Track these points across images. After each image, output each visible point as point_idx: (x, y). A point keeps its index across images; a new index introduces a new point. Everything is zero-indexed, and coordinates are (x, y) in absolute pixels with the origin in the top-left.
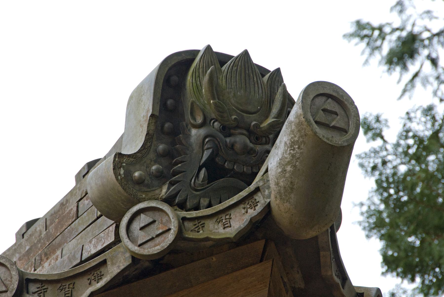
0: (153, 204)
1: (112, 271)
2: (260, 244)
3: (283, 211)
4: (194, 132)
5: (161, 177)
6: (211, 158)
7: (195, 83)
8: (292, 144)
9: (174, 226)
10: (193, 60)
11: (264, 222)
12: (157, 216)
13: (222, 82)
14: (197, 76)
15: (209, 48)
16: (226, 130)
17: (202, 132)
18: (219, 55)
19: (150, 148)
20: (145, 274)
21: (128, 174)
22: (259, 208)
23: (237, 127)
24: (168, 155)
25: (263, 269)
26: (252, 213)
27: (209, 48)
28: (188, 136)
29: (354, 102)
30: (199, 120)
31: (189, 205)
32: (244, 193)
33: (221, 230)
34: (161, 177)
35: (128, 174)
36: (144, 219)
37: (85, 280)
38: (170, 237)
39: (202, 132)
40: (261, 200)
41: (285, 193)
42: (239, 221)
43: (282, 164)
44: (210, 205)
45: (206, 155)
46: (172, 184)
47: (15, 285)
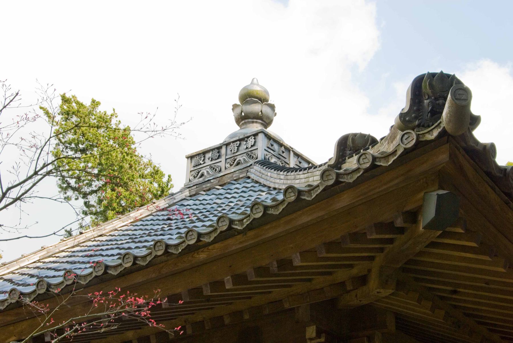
0: (408, 131)
1: (399, 153)
2: (446, 137)
3: (449, 129)
4: (425, 101)
5: (416, 118)
6: (432, 110)
7: (425, 85)
8: (449, 107)
9: (415, 137)
10: (424, 78)
11: (444, 133)
12: (410, 135)
13: (434, 83)
14: (425, 83)
15: (442, 72)
16: (436, 99)
17: (428, 101)
18: (431, 73)
19: (143, 218)
20: (407, 153)
21: (404, 119)
22: (441, 129)
23: (440, 97)
24: (418, 110)
25: (447, 146)
26: (439, 130)
27: (442, 72)
28: (424, 103)
29: (402, 116)
30: (427, 97)
31: (425, 125)
32: (436, 124)
33: (430, 137)
34: (416, 118)
35: (404, 119)
36: (406, 136)
37: (391, 157)
38: (414, 141)
39: (428, 101)
40: (442, 126)
41: (449, 121)
42: (435, 133)
43: (447, 114)
44: (433, 125)
45: (430, 108)
46: (419, 120)
47: (371, 160)
